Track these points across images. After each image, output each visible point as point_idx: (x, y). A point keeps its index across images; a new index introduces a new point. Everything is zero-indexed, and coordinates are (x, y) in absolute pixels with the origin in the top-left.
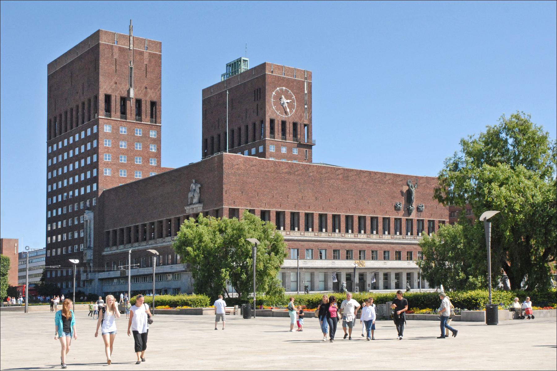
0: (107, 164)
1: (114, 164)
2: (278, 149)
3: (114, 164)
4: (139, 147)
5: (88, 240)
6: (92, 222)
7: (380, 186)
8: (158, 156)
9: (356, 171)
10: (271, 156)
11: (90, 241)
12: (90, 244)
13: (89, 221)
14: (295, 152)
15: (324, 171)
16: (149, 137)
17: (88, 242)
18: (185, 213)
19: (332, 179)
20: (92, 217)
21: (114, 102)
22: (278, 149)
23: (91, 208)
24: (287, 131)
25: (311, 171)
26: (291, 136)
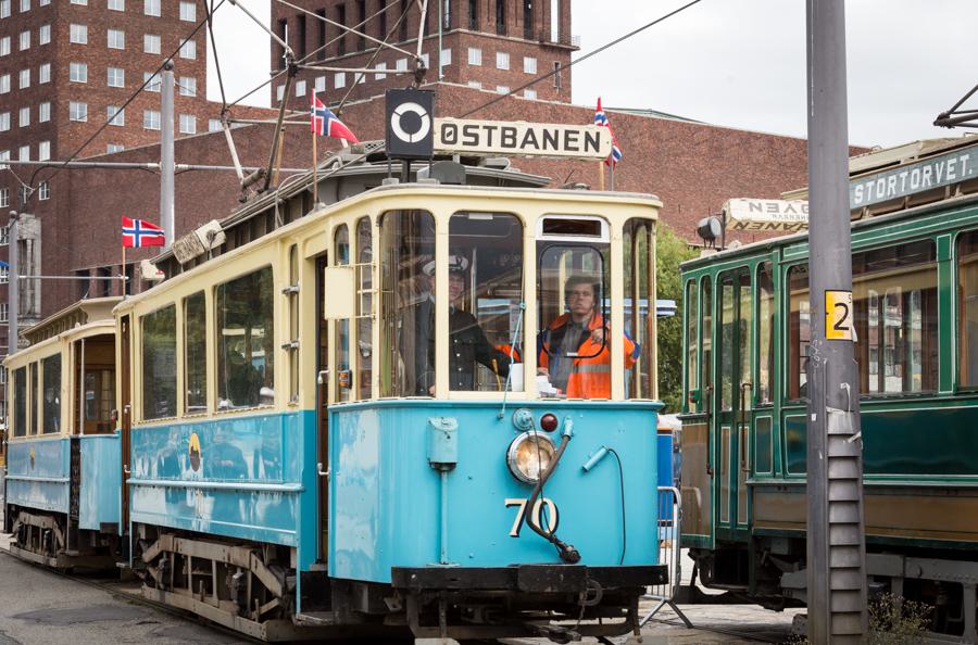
0: (78, 90)
1: (95, 91)
2: (489, 59)
3: (95, 91)
4: (116, 39)
5: (29, 293)
6: (38, 243)
7: (796, 175)
8: (197, 69)
9: (739, 133)
10: (472, 79)
11: (33, 296)
12: (33, 305)
13: (29, 242)
14: (530, 65)
15: (665, 134)
16: (178, 20)
17: (29, 300)
18: (38, 160)
19: (683, 153)
20: (39, 232)
21: (491, 8)
22: (489, 59)
23: (32, 207)
24: (511, 10)
25: (636, 131)
26: (521, 23)
